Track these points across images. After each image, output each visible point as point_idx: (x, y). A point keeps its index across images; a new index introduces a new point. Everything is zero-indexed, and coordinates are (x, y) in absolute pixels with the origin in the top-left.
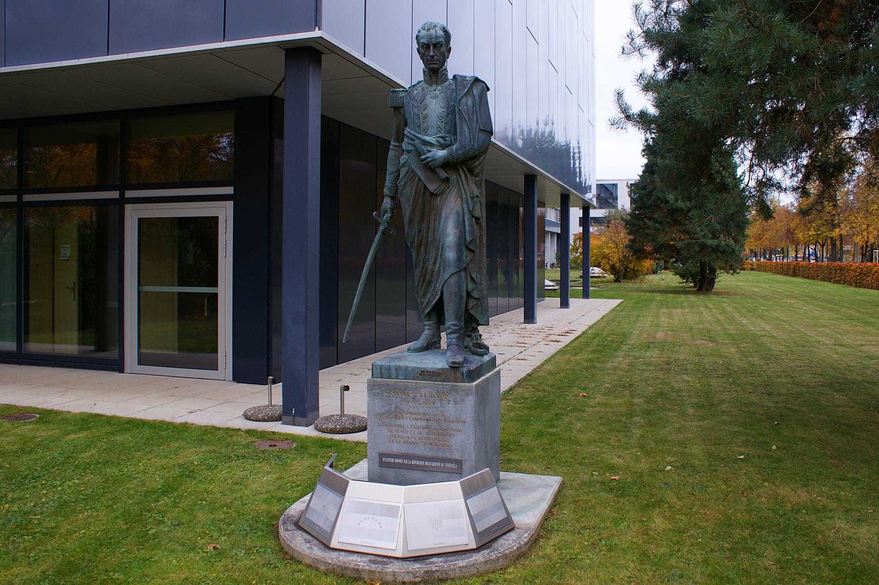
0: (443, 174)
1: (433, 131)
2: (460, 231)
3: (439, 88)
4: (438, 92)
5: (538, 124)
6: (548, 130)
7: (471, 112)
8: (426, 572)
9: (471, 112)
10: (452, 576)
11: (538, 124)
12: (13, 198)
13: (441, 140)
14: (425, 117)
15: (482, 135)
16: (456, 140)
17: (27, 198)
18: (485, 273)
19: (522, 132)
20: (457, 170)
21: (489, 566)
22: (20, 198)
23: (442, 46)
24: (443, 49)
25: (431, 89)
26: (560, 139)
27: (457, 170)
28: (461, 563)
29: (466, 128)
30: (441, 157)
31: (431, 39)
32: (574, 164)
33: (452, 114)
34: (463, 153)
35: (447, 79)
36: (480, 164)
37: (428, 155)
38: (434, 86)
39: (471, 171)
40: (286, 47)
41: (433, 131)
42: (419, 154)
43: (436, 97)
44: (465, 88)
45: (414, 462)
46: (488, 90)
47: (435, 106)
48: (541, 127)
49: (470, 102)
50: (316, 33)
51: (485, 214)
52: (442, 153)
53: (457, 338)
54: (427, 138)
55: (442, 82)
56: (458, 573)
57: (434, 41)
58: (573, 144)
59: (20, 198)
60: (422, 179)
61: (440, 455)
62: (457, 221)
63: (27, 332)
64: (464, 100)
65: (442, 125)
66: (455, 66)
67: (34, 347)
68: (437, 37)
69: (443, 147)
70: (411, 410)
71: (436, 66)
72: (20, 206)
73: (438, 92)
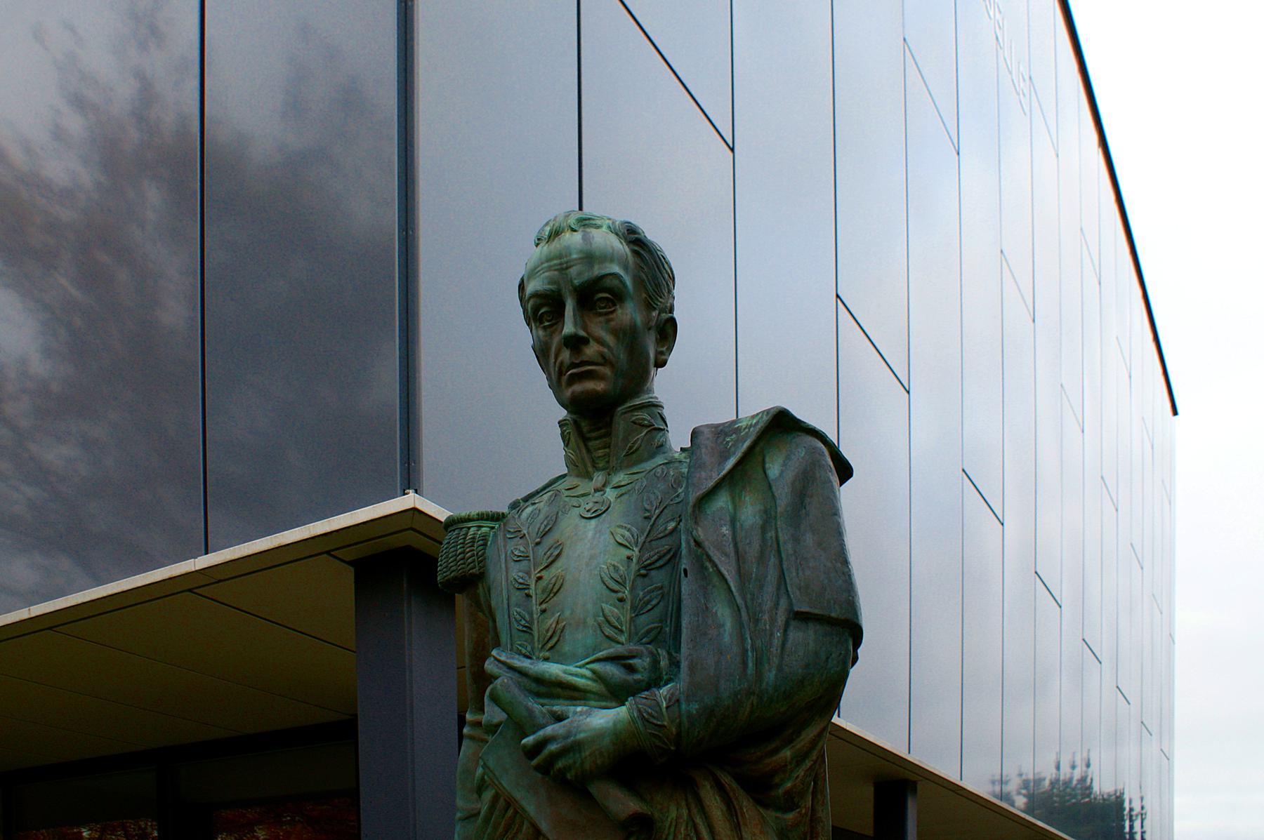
0: (622, 803)
1: (580, 639)
3: (621, 478)
4: (610, 494)
5: (1058, 768)
6: (1077, 774)
7: (753, 551)
9: (753, 551)
11: (1058, 768)
13: (611, 670)
14: (553, 591)
15: (804, 640)
16: (675, 664)
19: (1026, 784)
23: (617, 297)
24: (629, 313)
25: (585, 486)
26: (1103, 786)
27: (688, 787)
29: (723, 613)
30: (600, 734)
31: (563, 268)
32: (1131, 827)
33: (664, 567)
35: (661, 447)
36: (801, 758)
37: (549, 730)
38: (599, 478)
39: (760, 788)
40: (350, 554)
41: (580, 639)
42: (521, 726)
44: (724, 457)
46: (845, 471)
47: (594, 546)
48: (1065, 772)
49: (750, 512)
50: (409, 500)
52: (601, 719)
54: (554, 669)
55: (633, 457)
57: (578, 274)
58: (1132, 799)
60: (544, 827)
64: (722, 501)
65: (619, 614)
66: (695, 392)
68: (590, 258)
69: (615, 694)
71: (599, 386)
73: (610, 494)
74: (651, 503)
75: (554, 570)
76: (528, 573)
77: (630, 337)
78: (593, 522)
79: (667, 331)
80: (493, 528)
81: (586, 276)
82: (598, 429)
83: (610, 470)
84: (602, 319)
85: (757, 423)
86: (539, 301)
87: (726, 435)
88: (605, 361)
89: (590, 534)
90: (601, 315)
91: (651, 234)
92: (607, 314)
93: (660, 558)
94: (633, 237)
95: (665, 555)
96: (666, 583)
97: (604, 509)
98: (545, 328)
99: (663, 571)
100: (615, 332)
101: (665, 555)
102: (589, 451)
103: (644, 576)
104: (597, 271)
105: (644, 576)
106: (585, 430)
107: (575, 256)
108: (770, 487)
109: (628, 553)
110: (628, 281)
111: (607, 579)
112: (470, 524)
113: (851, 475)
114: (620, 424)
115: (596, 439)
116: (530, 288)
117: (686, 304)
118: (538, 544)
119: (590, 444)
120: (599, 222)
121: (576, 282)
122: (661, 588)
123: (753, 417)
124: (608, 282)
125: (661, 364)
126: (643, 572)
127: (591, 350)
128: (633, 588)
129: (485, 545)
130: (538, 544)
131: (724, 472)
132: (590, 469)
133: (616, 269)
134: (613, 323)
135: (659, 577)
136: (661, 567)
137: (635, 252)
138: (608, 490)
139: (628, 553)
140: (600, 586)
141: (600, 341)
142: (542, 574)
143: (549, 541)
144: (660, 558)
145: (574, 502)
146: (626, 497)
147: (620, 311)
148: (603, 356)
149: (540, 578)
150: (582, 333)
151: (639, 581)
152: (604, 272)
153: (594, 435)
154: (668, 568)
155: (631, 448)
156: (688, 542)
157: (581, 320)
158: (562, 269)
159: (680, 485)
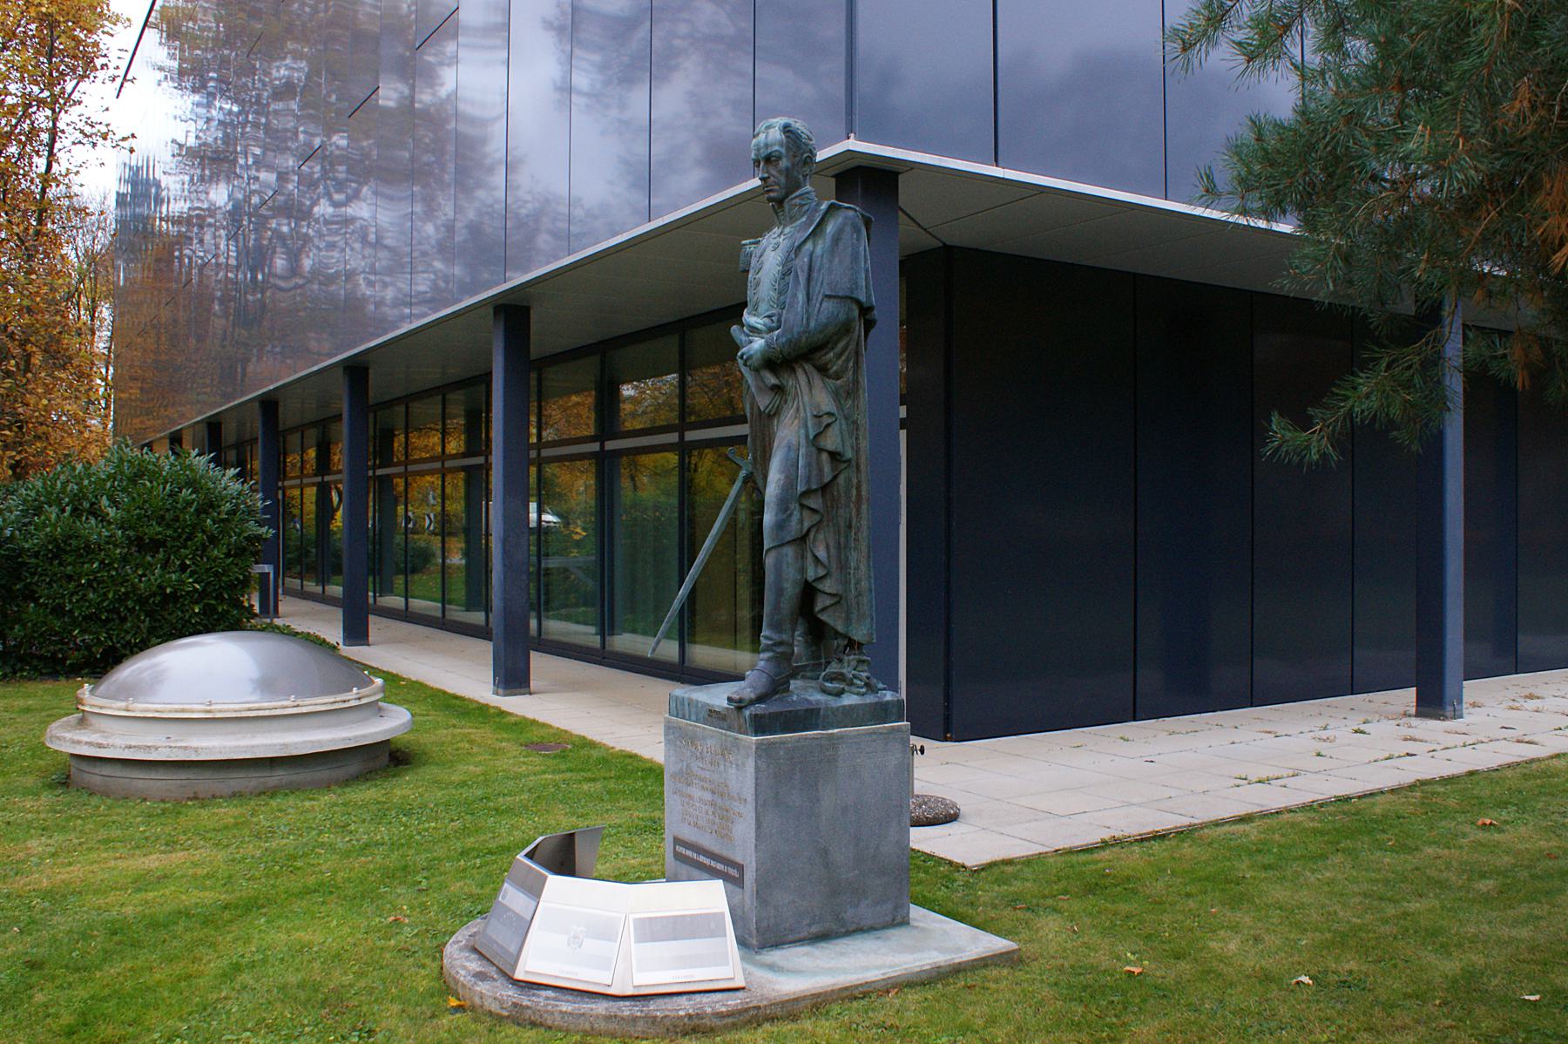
2: (787, 477)
8: (515, 1005)
10: (549, 1023)
12: (673, 438)
17: (691, 436)
18: (864, 549)
20: (794, 370)
21: (612, 1026)
22: (682, 437)
23: (779, 158)
28: (565, 1007)
34: (789, 341)
39: (823, 370)
41: (763, 307)
45: (702, 859)
51: (865, 445)
53: (768, 660)
56: (558, 1021)
59: (682, 437)
61: (724, 853)
62: (787, 458)
63: (693, 626)
67: (624, 642)
70: (700, 773)
72: (684, 449)
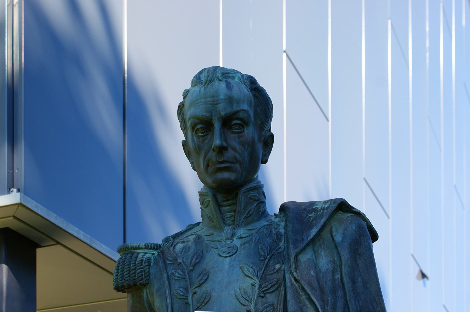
3: (241, 232)
4: (237, 242)
23: (244, 123)
31: (215, 103)
38: (228, 230)
43: (233, 252)
49: (324, 262)
57: (223, 109)
66: (287, 180)
68: (230, 100)
74: (264, 251)
75: (204, 288)
76: (186, 289)
77: (252, 145)
78: (228, 259)
79: (268, 142)
80: (153, 254)
81: (229, 110)
82: (229, 200)
83: (235, 225)
84: (236, 136)
85: (328, 207)
86: (196, 121)
87: (308, 212)
88: (236, 161)
89: (227, 267)
90: (235, 133)
91: (261, 83)
92: (238, 133)
93: (272, 286)
94: (254, 86)
95: (274, 285)
96: (276, 303)
97: (234, 251)
98: (199, 137)
99: (274, 294)
100: (243, 144)
101: (274, 285)
102: (221, 213)
103: (262, 297)
104: (235, 108)
105: (262, 297)
106: (220, 200)
107: (222, 97)
108: (336, 247)
109: (252, 281)
110: (252, 114)
111: (240, 297)
112: (139, 251)
113: (377, 239)
114: (242, 199)
115: (226, 206)
116: (189, 113)
117: (280, 125)
118: (192, 270)
119: (222, 208)
120: (233, 75)
121: (223, 113)
122: (272, 305)
123: (327, 201)
124: (241, 115)
125: (265, 162)
126: (262, 295)
127: (230, 154)
128: (256, 304)
129: (149, 265)
130: (192, 270)
131: (311, 237)
132: (222, 224)
133: (245, 106)
134: (242, 139)
135: (271, 298)
136: (272, 292)
137: (254, 96)
138: (235, 239)
139: (252, 281)
140: (235, 301)
141: (234, 149)
142: (197, 289)
143: (198, 270)
144: (272, 286)
145: (212, 245)
146: (247, 245)
147: (246, 132)
148: (235, 158)
149: (195, 293)
150: (224, 144)
151: (260, 300)
152: (238, 109)
153: (225, 203)
154: (277, 292)
155: (248, 214)
156: (290, 280)
157: (224, 137)
158: (214, 104)
159: (280, 240)
